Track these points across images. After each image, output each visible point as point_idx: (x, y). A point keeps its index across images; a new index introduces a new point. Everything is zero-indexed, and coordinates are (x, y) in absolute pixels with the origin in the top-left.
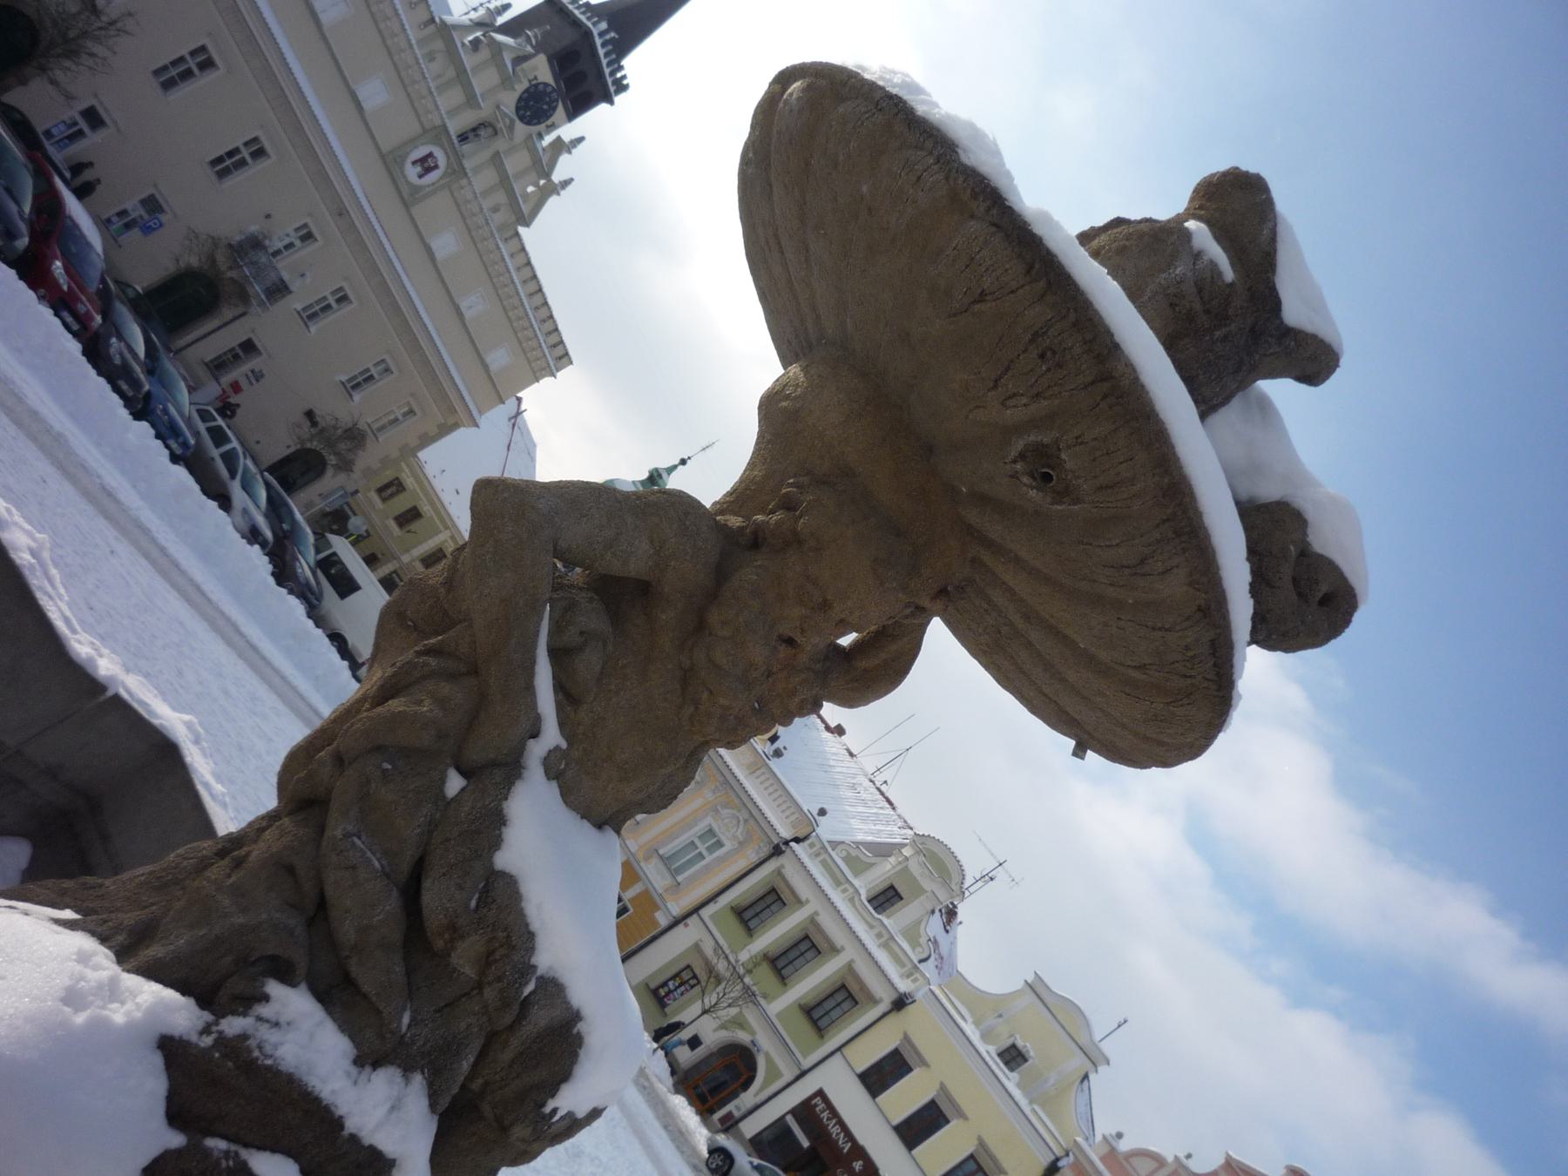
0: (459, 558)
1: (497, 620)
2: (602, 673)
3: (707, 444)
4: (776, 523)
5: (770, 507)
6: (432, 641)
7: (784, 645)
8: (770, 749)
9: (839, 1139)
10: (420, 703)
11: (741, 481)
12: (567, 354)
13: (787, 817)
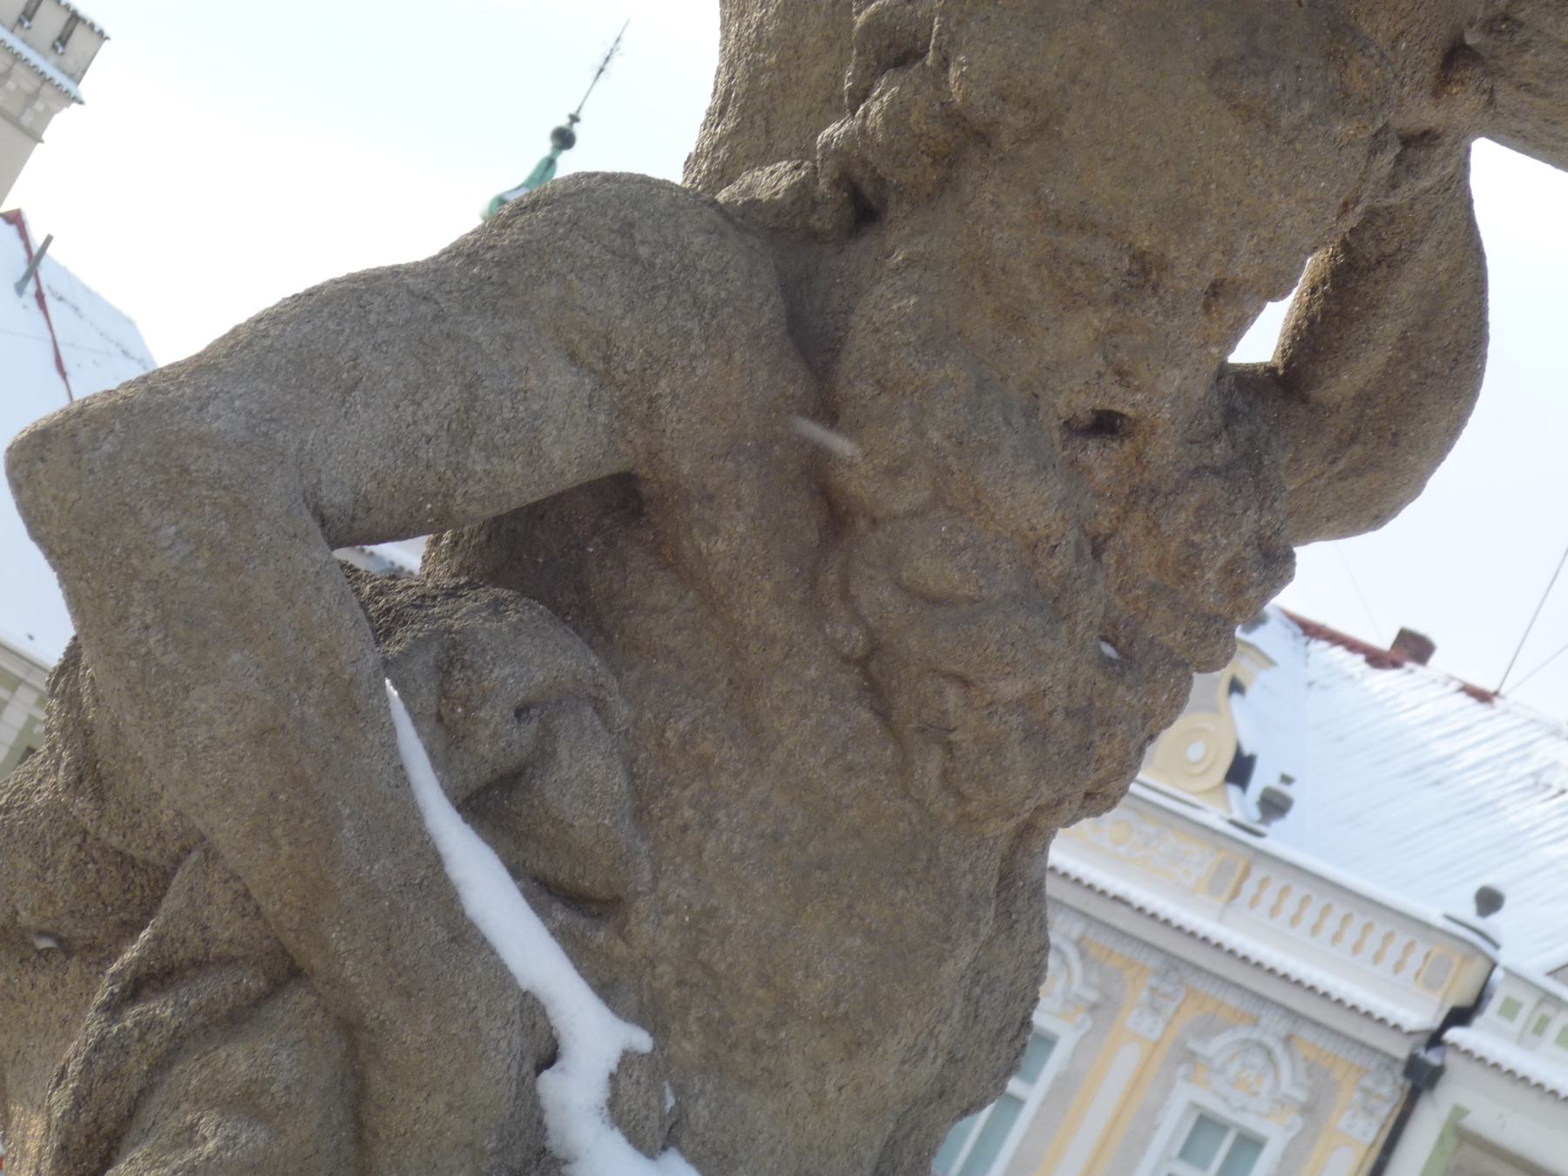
0: (78, 695)
1: (273, 795)
2: (637, 792)
4: (887, 121)
5: (847, 85)
6: (131, 953)
7: (1092, 443)
8: (1243, 804)
10: (188, 1136)
12: (75, 18)
13: (1398, 967)
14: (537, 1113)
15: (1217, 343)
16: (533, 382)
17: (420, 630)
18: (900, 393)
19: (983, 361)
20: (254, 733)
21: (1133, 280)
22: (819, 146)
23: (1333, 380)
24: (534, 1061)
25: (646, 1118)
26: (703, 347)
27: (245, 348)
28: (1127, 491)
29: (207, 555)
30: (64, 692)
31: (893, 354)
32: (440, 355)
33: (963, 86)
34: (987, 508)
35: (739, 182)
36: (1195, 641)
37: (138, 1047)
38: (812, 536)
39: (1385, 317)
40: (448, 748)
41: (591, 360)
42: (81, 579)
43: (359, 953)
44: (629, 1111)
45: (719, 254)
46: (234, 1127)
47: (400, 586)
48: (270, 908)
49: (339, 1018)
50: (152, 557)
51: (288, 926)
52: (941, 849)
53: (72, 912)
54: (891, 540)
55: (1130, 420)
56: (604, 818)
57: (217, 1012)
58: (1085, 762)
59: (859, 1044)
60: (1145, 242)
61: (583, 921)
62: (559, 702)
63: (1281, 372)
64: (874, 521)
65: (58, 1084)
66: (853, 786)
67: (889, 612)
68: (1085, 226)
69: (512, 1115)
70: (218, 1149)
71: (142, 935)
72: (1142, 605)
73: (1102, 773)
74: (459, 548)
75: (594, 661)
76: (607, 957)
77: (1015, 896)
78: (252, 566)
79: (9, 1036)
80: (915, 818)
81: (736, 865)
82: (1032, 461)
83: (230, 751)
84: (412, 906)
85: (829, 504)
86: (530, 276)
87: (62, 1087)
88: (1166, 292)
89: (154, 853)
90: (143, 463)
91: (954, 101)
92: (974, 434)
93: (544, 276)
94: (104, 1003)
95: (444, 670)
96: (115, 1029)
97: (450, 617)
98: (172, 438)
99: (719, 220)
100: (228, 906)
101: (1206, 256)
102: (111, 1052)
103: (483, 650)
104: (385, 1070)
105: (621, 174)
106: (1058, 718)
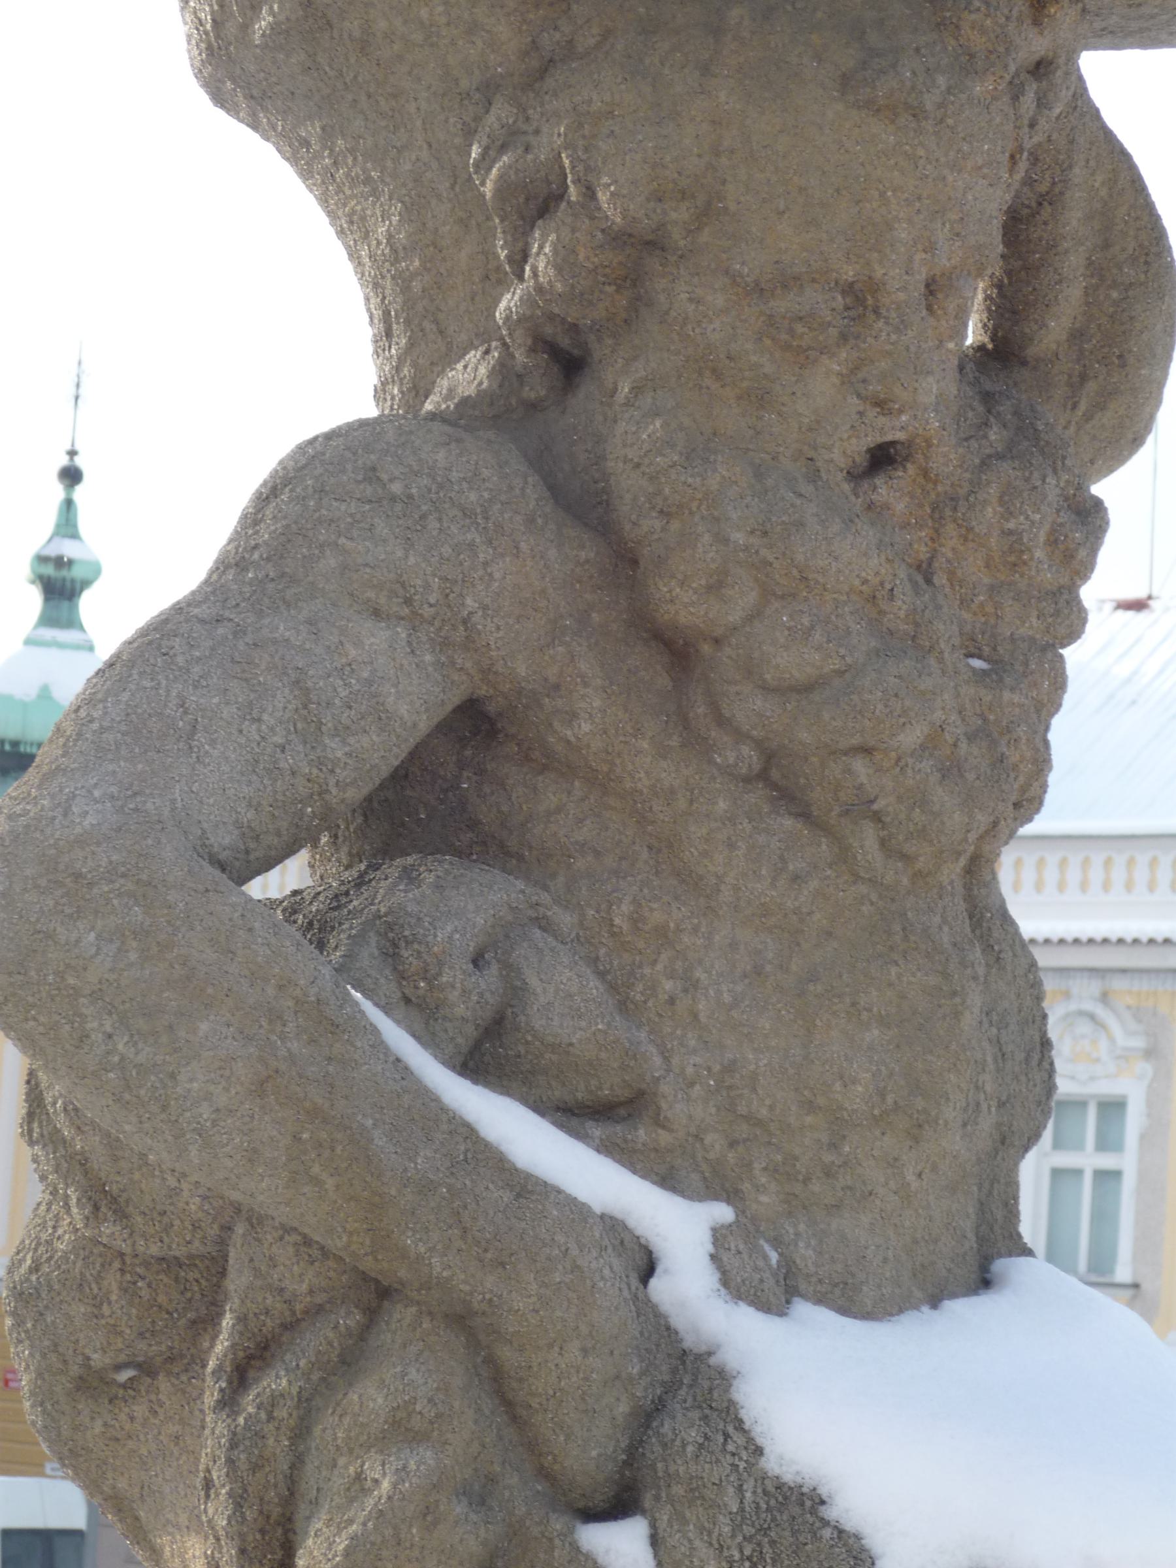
0: (58, 1131)
1: (296, 1138)
2: (613, 988)
4: (559, 269)
6: (222, 1345)
7: (879, 481)
10: (359, 1485)
11: (374, 285)
14: (662, 1322)
15: (951, 338)
16: (353, 653)
17: (351, 928)
18: (687, 512)
19: (748, 449)
20: (253, 1088)
21: (853, 313)
22: (501, 322)
23: (1042, 332)
24: (636, 1275)
25: (762, 1281)
26: (491, 551)
27: (76, 740)
28: (929, 511)
29: (134, 944)
30: (42, 1135)
31: (663, 480)
32: (257, 666)
33: (618, 205)
34: (817, 582)
35: (437, 390)
36: (1050, 620)
37: (271, 1426)
38: (664, 681)
39: (1066, 252)
40: (427, 1024)
41: (395, 609)
42: (27, 1020)
43: (439, 1247)
44: (743, 1281)
45: (464, 459)
46: (399, 1459)
47: (308, 898)
48: (336, 1244)
49: (447, 1316)
50: (85, 969)
51: (362, 1252)
52: (910, 914)
53: (141, 1334)
54: (741, 651)
55: (903, 443)
56: (597, 1024)
57: (329, 1361)
58: (1005, 776)
59: (920, 1126)
60: (849, 273)
61: (619, 1128)
62: (507, 936)
63: (990, 346)
64: (717, 641)
65: (208, 1496)
66: (806, 893)
67: (768, 718)
68: (788, 282)
69: (642, 1333)
70: (395, 1486)
71: (224, 1324)
72: (989, 609)
73: (1022, 779)
74: (341, 839)
75: (520, 884)
76: (656, 1150)
77: (989, 929)
78: (180, 935)
79: (127, 1476)
80: (874, 897)
81: (734, 1013)
82: (837, 520)
83: (239, 1114)
84: (467, 1182)
85: (666, 644)
86: (305, 557)
87: (213, 1496)
88: (888, 310)
89: (197, 1243)
90: (37, 886)
91: (613, 223)
92: (774, 519)
93: (317, 552)
94: (218, 1401)
95: (391, 954)
96: (241, 1420)
97: (372, 904)
98: (53, 851)
99: (447, 429)
100: (294, 1260)
101: (911, 260)
102: (247, 1443)
103: (419, 919)
104: (511, 1343)
105: (340, 428)
106: (963, 746)
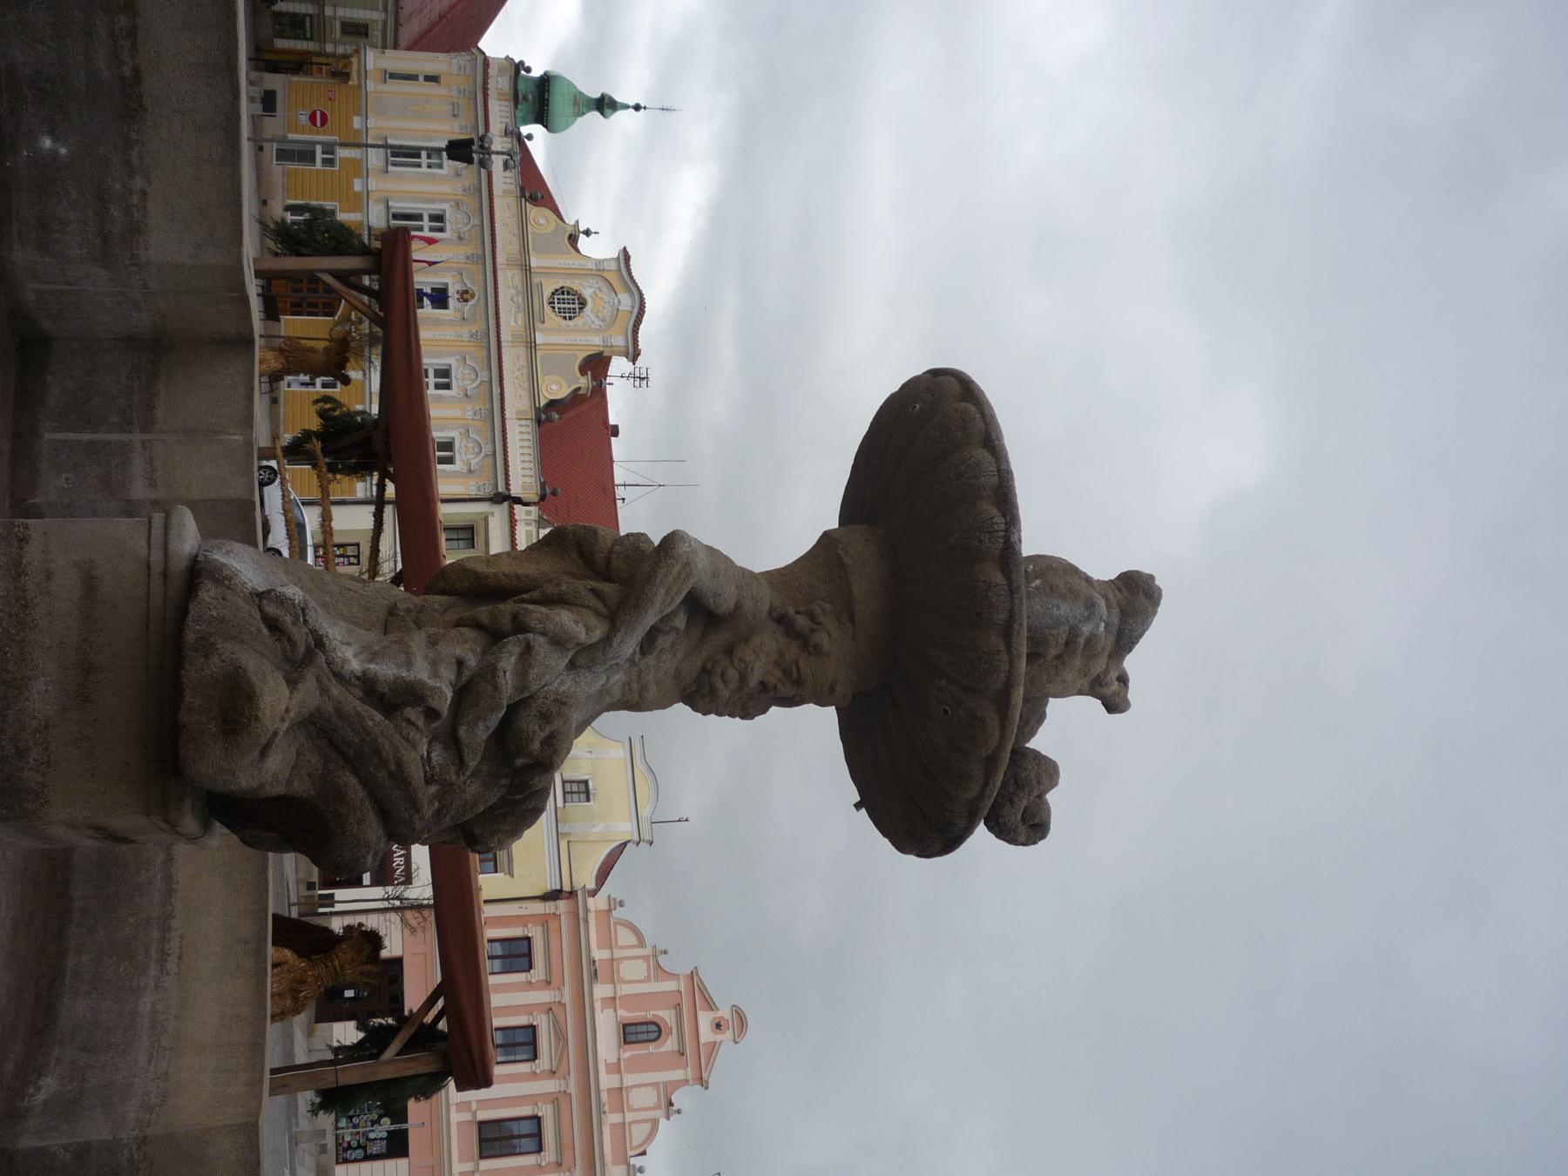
3: (669, 108)
9: (398, 869)
